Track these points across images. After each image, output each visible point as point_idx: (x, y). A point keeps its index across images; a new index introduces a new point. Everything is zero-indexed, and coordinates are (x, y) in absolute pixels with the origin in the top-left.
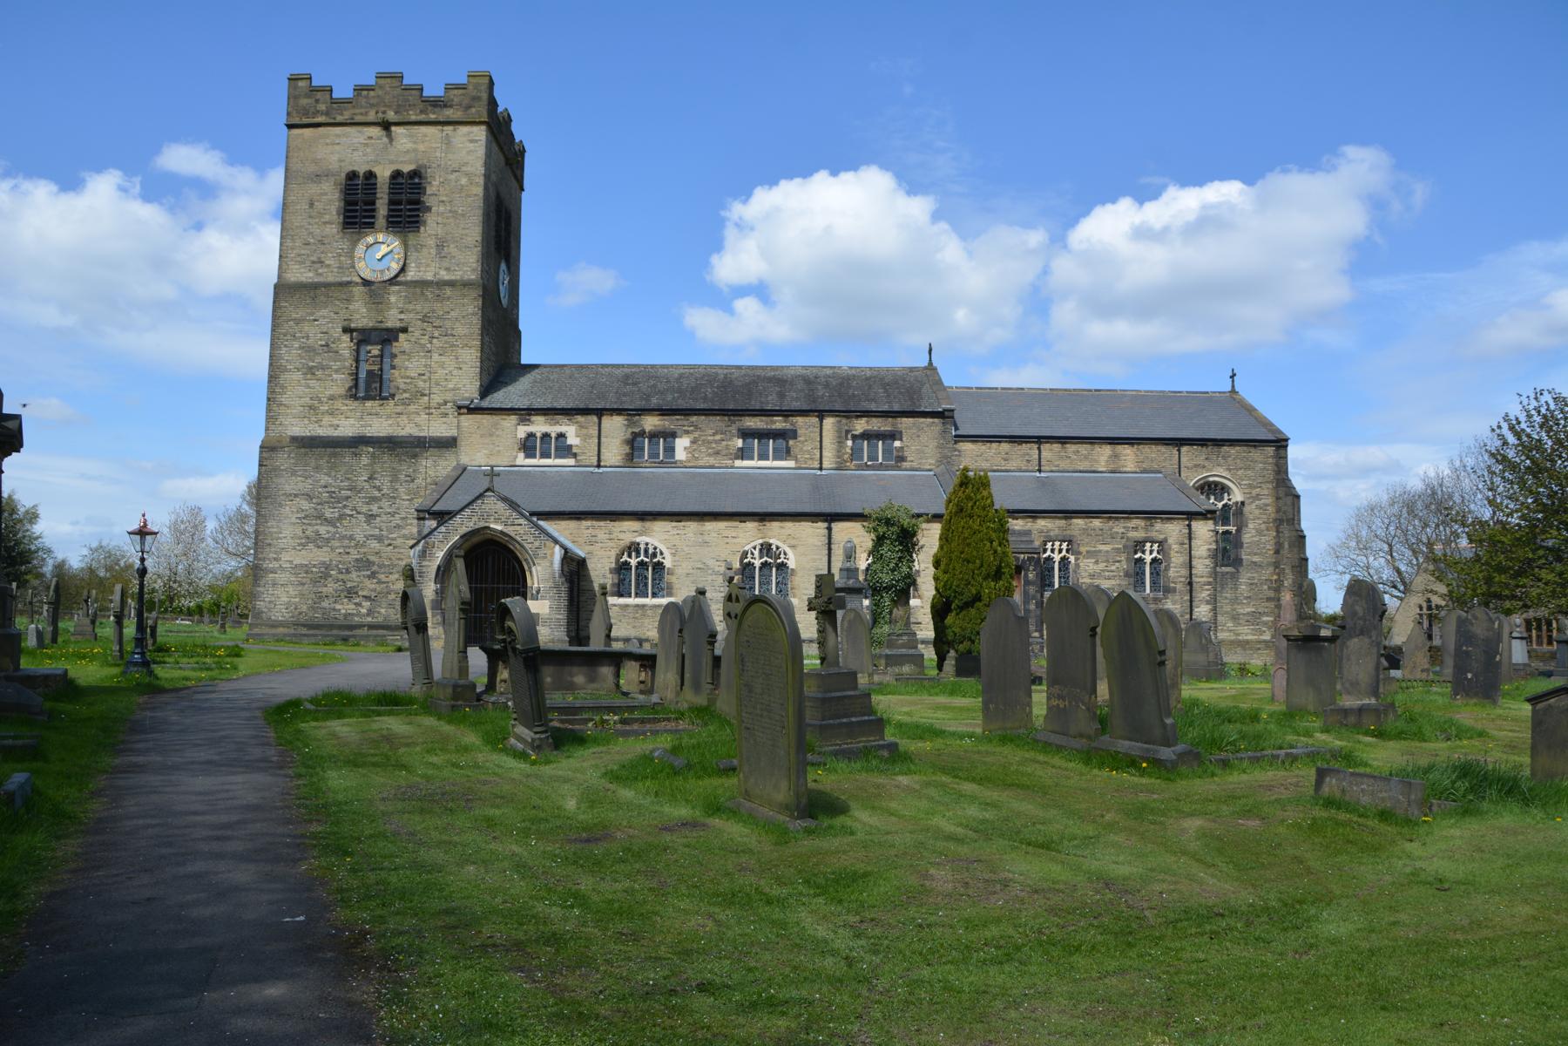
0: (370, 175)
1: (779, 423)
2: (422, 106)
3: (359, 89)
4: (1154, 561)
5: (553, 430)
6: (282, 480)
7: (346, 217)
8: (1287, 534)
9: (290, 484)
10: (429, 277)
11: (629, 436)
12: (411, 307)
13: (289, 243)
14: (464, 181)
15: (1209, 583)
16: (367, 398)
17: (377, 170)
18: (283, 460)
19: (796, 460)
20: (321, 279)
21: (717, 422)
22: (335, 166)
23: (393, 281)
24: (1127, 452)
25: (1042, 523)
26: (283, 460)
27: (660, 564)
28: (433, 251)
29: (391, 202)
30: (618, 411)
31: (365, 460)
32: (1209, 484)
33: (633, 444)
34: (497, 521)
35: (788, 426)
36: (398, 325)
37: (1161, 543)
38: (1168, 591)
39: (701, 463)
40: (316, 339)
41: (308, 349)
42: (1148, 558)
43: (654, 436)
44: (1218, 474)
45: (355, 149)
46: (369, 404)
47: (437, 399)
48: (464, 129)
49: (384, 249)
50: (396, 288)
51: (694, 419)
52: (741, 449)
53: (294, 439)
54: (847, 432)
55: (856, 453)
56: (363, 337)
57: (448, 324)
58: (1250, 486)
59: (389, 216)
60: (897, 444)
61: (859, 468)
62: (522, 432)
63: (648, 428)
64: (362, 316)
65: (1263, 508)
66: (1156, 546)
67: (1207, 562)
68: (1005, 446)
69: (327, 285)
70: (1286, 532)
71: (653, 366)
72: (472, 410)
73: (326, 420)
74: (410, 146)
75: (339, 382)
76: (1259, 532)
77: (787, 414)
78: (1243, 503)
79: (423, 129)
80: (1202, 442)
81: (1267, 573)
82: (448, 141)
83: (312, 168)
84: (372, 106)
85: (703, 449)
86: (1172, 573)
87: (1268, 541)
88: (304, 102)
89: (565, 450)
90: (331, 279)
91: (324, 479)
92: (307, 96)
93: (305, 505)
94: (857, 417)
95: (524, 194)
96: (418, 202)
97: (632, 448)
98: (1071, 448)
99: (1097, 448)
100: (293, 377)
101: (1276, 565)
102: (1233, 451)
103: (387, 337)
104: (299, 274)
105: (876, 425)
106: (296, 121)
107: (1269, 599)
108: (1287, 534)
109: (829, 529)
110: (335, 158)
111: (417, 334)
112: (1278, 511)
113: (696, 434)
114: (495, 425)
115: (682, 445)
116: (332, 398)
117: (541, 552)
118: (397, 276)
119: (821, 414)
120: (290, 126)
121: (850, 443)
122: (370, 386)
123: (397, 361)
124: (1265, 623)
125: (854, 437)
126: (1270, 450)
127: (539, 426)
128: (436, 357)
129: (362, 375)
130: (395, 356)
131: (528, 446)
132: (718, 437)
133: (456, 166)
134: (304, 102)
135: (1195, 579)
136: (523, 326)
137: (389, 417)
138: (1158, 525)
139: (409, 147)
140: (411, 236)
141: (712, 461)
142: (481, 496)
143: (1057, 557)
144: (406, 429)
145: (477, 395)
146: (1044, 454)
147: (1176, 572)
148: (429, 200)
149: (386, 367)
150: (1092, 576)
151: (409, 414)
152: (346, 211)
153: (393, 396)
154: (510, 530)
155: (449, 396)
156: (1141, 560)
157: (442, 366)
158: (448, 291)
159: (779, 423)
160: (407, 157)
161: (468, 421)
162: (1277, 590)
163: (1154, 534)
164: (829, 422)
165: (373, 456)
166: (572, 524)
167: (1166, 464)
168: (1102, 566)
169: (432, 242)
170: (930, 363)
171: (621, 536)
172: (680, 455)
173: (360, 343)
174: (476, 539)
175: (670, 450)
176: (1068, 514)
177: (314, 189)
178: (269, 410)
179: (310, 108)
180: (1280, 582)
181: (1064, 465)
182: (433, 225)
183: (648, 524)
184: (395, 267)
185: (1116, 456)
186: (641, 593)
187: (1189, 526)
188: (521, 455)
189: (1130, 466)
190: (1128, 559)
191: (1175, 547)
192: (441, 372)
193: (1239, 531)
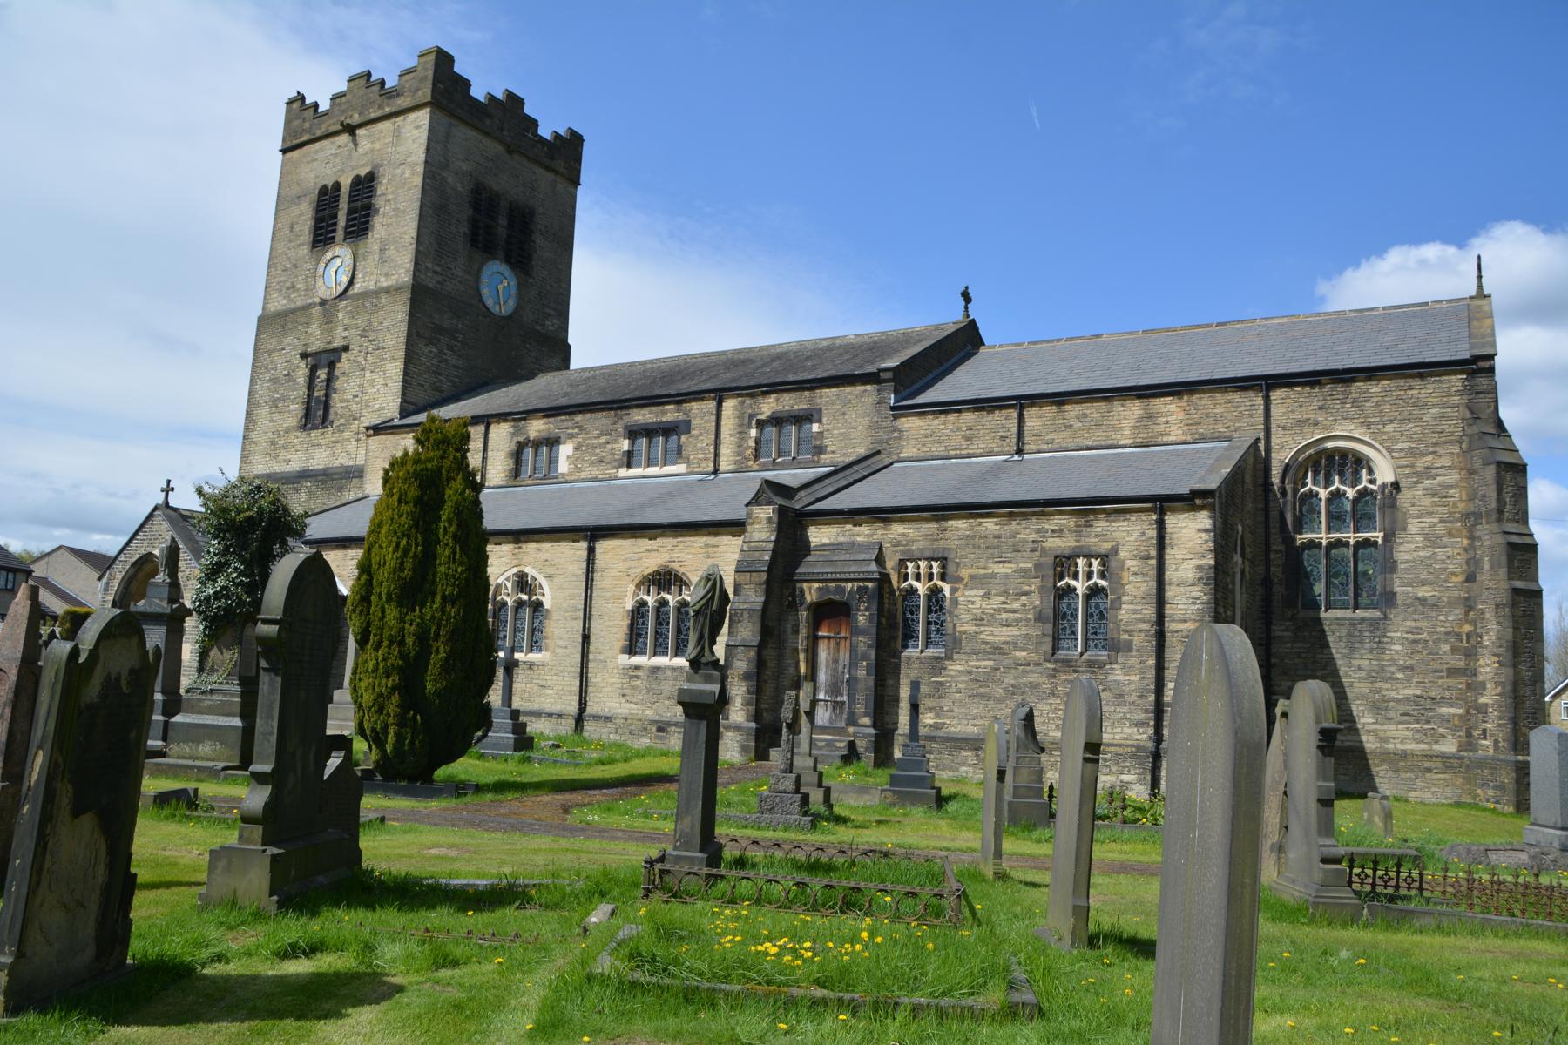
1: (670, 414)
3: (334, 98)
4: (1095, 591)
7: (315, 236)
8: (1487, 541)
11: (514, 447)
16: (315, 428)
17: (342, 180)
19: (688, 462)
20: (292, 305)
21: (602, 419)
24: (1171, 409)
25: (898, 529)
27: (539, 604)
29: (350, 211)
30: (502, 417)
32: (1330, 455)
35: (681, 417)
37: (1105, 558)
38: (1116, 647)
39: (583, 475)
40: (282, 369)
42: (1080, 586)
43: (537, 444)
44: (1347, 433)
45: (333, 163)
48: (412, 116)
51: (579, 418)
52: (629, 454)
58: (1411, 452)
59: (347, 227)
60: (815, 427)
63: (533, 435)
64: (316, 345)
65: (1441, 493)
66: (1095, 563)
67: (1196, 591)
68: (968, 417)
69: (293, 311)
70: (1490, 538)
73: (283, 454)
74: (369, 146)
75: (297, 409)
76: (1432, 540)
78: (1396, 486)
83: (295, 190)
86: (1124, 614)
87: (1452, 556)
90: (299, 304)
94: (765, 394)
96: (369, 207)
98: (1073, 410)
99: (1118, 407)
100: (263, 411)
101: (1469, 605)
102: (1375, 389)
104: (279, 304)
105: (790, 402)
106: (289, 144)
107: (1452, 672)
108: (1487, 541)
109: (591, 550)
112: (1471, 499)
115: (566, 450)
121: (753, 433)
122: (317, 414)
124: (1447, 720)
126: (1456, 381)
128: (368, 374)
132: (603, 439)
135: (1170, 626)
136: (572, 339)
138: (1101, 525)
139: (374, 145)
140: (361, 244)
141: (594, 471)
147: (1132, 611)
148: (379, 202)
150: (978, 620)
156: (1070, 590)
158: (384, 299)
159: (670, 414)
162: (1471, 654)
163: (1091, 542)
165: (310, 492)
167: (1243, 423)
168: (996, 601)
169: (376, 248)
172: (563, 467)
173: (313, 370)
175: (553, 461)
178: (243, 449)
181: (1061, 438)
182: (380, 227)
184: (345, 280)
185: (1150, 417)
186: (659, 650)
187: (1161, 526)
189: (1176, 433)
190: (1042, 589)
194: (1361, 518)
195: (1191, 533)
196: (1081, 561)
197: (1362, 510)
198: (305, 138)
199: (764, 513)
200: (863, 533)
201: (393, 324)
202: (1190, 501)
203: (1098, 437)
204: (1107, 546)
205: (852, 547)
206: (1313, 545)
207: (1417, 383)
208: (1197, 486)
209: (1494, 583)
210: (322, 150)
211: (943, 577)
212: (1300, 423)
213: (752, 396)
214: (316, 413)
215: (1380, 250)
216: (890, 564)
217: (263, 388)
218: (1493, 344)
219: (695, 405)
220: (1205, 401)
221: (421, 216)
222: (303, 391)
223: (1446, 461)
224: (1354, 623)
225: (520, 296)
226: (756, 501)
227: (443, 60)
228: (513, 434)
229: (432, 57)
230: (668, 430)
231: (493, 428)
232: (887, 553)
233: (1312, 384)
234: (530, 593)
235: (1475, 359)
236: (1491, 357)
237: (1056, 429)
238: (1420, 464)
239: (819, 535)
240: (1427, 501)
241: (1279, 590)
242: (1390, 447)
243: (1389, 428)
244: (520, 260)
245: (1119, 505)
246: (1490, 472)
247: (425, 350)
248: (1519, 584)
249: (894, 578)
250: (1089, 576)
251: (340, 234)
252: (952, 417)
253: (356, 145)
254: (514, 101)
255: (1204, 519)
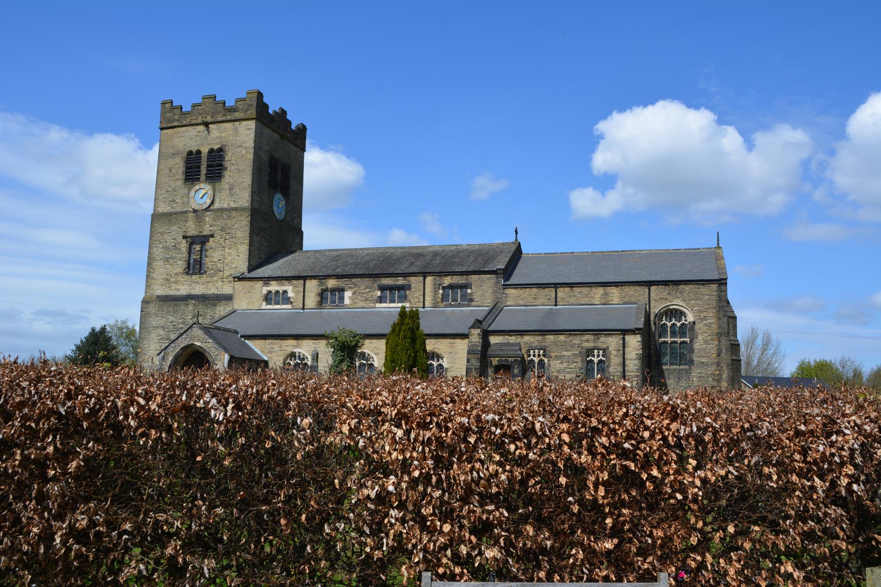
0: (199, 152)
1: (401, 281)
2: (224, 112)
3: (194, 106)
4: (600, 361)
5: (281, 289)
6: (151, 319)
9: (155, 321)
10: (225, 206)
11: (320, 291)
12: (216, 223)
13: (159, 192)
14: (244, 152)
15: (637, 376)
16: (194, 274)
18: (152, 308)
19: (410, 302)
20: (174, 210)
21: (367, 281)
22: (181, 149)
23: (207, 209)
24: (614, 292)
25: (527, 338)
26: (152, 308)
27: (372, 365)
28: (227, 192)
29: (208, 166)
31: (191, 308)
33: (322, 295)
34: (198, 340)
35: (406, 283)
36: (209, 233)
37: (604, 350)
39: (358, 306)
40: (170, 243)
41: (167, 248)
42: (596, 360)
43: (333, 291)
44: (677, 303)
45: (192, 139)
46: (194, 277)
47: (227, 273)
48: (244, 123)
49: (203, 192)
50: (209, 213)
51: (354, 280)
52: (380, 297)
53: (158, 297)
54: (440, 285)
55: (444, 298)
56: (192, 241)
57: (233, 231)
58: (699, 311)
59: (207, 174)
60: (469, 291)
61: (446, 306)
62: (265, 290)
63: (330, 286)
64: (192, 231)
65: (709, 326)
66: (601, 352)
67: (636, 362)
68: (535, 290)
69: (176, 213)
70: (725, 342)
71: (356, 249)
72: (240, 278)
73: (174, 286)
74: (218, 134)
75: (181, 265)
76: (706, 342)
77: (405, 275)
78: (694, 323)
79: (225, 125)
80: (665, 283)
81: (712, 369)
82: (236, 130)
83: (171, 151)
84: (200, 114)
85: (359, 298)
86: (611, 369)
88: (168, 115)
89: (288, 301)
90: (178, 210)
91: (171, 318)
92: (170, 112)
93: (162, 332)
94: (446, 276)
95: (306, 154)
96: (221, 165)
97: (322, 298)
98: (577, 290)
99: (594, 289)
100: (159, 264)
101: (718, 364)
102: (687, 288)
103: (203, 240)
104: (164, 208)
106: (164, 126)
110: (182, 144)
111: (218, 238)
112: (719, 327)
113: (355, 289)
114: (252, 287)
115: (348, 294)
116: (176, 274)
117: (218, 357)
118: (210, 206)
119: (425, 275)
120: (162, 129)
121: (441, 291)
122: (195, 267)
123: (208, 253)
125: (444, 288)
126: (714, 287)
127: (274, 287)
128: (227, 250)
129: (192, 261)
130: (207, 250)
131: (268, 298)
132: (367, 290)
133: (240, 144)
134: (168, 115)
137: (203, 284)
138: (603, 339)
139: (219, 135)
140: (217, 184)
141: (363, 304)
142: (191, 327)
143: (536, 360)
144: (212, 290)
145: (246, 270)
146: (559, 294)
148: (227, 164)
149: (203, 256)
150: (559, 372)
151: (213, 282)
152: (187, 172)
153: (205, 272)
154: (204, 346)
155: (232, 272)
156: (592, 361)
157: (230, 255)
158: (234, 213)
159: (401, 281)
160: (216, 141)
161: (239, 285)
163: (599, 345)
164: (429, 279)
165: (195, 305)
166: (262, 342)
168: (565, 365)
169: (227, 187)
170: (516, 240)
171: (286, 348)
172: (347, 301)
173: (191, 244)
174: (189, 350)
175: (342, 299)
176: (543, 332)
177: (171, 162)
178: (147, 282)
179: (172, 117)
180: (720, 375)
181: (571, 301)
182: (228, 177)
183: (300, 341)
184: (209, 201)
185: (606, 294)
187: (624, 339)
188: (264, 303)
189: (616, 300)
190: (582, 361)
191: (614, 353)
192: (229, 258)
193: (691, 341)
194: (683, 334)
195: (634, 343)
196: (596, 351)
197: (683, 331)
198: (176, 124)
199: (476, 332)
200: (513, 339)
201: (241, 227)
202: (633, 332)
203: (586, 300)
204: (605, 346)
205: (508, 344)
206: (665, 342)
207: (701, 287)
208: (636, 326)
209: (726, 357)
210: (188, 132)
211: (544, 356)
212: (661, 299)
213: (440, 276)
214: (195, 267)
215: (647, 100)
216: (523, 351)
217: (158, 252)
218: (726, 274)
219: (413, 278)
220: (627, 289)
221: (253, 174)
222: (186, 255)
223: (711, 315)
224: (680, 370)
225: (287, 211)
226: (473, 327)
227: (260, 95)
228: (319, 285)
229: (256, 95)
230: (400, 288)
231: (307, 282)
232: (522, 347)
233: (665, 285)
234: (367, 360)
235: (721, 280)
236: (726, 279)
237: (570, 297)
238: (702, 315)
239: (494, 340)
240: (705, 328)
241: (654, 359)
242: (693, 309)
243: (692, 302)
244: (286, 194)
245: (609, 332)
246: (725, 319)
247: (256, 239)
248: (734, 358)
249: (526, 356)
250: (598, 356)
251: (203, 177)
252: (528, 290)
253: (209, 132)
254: (284, 112)
255: (638, 338)
